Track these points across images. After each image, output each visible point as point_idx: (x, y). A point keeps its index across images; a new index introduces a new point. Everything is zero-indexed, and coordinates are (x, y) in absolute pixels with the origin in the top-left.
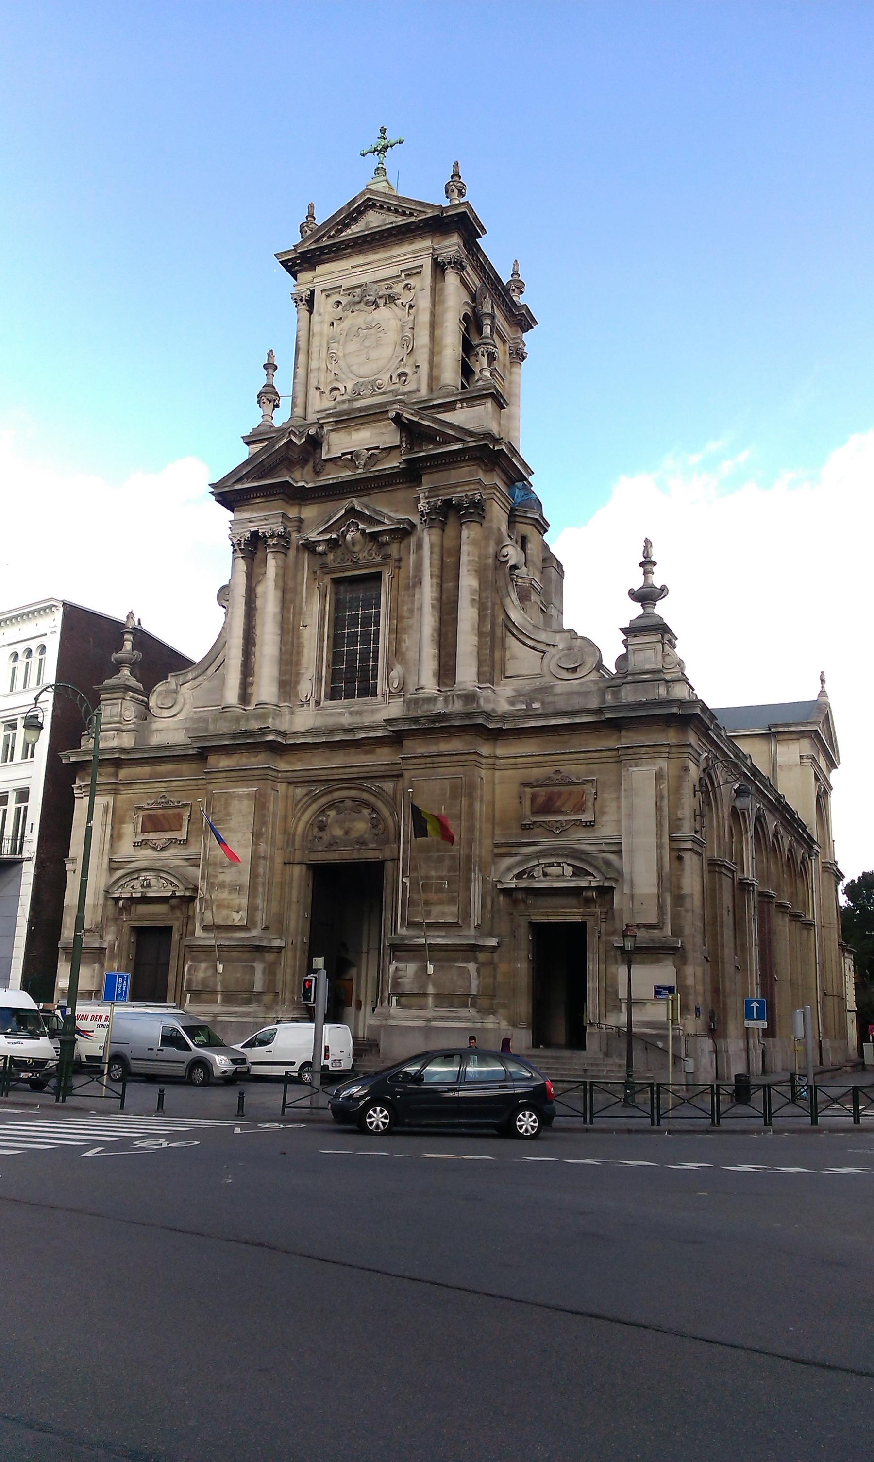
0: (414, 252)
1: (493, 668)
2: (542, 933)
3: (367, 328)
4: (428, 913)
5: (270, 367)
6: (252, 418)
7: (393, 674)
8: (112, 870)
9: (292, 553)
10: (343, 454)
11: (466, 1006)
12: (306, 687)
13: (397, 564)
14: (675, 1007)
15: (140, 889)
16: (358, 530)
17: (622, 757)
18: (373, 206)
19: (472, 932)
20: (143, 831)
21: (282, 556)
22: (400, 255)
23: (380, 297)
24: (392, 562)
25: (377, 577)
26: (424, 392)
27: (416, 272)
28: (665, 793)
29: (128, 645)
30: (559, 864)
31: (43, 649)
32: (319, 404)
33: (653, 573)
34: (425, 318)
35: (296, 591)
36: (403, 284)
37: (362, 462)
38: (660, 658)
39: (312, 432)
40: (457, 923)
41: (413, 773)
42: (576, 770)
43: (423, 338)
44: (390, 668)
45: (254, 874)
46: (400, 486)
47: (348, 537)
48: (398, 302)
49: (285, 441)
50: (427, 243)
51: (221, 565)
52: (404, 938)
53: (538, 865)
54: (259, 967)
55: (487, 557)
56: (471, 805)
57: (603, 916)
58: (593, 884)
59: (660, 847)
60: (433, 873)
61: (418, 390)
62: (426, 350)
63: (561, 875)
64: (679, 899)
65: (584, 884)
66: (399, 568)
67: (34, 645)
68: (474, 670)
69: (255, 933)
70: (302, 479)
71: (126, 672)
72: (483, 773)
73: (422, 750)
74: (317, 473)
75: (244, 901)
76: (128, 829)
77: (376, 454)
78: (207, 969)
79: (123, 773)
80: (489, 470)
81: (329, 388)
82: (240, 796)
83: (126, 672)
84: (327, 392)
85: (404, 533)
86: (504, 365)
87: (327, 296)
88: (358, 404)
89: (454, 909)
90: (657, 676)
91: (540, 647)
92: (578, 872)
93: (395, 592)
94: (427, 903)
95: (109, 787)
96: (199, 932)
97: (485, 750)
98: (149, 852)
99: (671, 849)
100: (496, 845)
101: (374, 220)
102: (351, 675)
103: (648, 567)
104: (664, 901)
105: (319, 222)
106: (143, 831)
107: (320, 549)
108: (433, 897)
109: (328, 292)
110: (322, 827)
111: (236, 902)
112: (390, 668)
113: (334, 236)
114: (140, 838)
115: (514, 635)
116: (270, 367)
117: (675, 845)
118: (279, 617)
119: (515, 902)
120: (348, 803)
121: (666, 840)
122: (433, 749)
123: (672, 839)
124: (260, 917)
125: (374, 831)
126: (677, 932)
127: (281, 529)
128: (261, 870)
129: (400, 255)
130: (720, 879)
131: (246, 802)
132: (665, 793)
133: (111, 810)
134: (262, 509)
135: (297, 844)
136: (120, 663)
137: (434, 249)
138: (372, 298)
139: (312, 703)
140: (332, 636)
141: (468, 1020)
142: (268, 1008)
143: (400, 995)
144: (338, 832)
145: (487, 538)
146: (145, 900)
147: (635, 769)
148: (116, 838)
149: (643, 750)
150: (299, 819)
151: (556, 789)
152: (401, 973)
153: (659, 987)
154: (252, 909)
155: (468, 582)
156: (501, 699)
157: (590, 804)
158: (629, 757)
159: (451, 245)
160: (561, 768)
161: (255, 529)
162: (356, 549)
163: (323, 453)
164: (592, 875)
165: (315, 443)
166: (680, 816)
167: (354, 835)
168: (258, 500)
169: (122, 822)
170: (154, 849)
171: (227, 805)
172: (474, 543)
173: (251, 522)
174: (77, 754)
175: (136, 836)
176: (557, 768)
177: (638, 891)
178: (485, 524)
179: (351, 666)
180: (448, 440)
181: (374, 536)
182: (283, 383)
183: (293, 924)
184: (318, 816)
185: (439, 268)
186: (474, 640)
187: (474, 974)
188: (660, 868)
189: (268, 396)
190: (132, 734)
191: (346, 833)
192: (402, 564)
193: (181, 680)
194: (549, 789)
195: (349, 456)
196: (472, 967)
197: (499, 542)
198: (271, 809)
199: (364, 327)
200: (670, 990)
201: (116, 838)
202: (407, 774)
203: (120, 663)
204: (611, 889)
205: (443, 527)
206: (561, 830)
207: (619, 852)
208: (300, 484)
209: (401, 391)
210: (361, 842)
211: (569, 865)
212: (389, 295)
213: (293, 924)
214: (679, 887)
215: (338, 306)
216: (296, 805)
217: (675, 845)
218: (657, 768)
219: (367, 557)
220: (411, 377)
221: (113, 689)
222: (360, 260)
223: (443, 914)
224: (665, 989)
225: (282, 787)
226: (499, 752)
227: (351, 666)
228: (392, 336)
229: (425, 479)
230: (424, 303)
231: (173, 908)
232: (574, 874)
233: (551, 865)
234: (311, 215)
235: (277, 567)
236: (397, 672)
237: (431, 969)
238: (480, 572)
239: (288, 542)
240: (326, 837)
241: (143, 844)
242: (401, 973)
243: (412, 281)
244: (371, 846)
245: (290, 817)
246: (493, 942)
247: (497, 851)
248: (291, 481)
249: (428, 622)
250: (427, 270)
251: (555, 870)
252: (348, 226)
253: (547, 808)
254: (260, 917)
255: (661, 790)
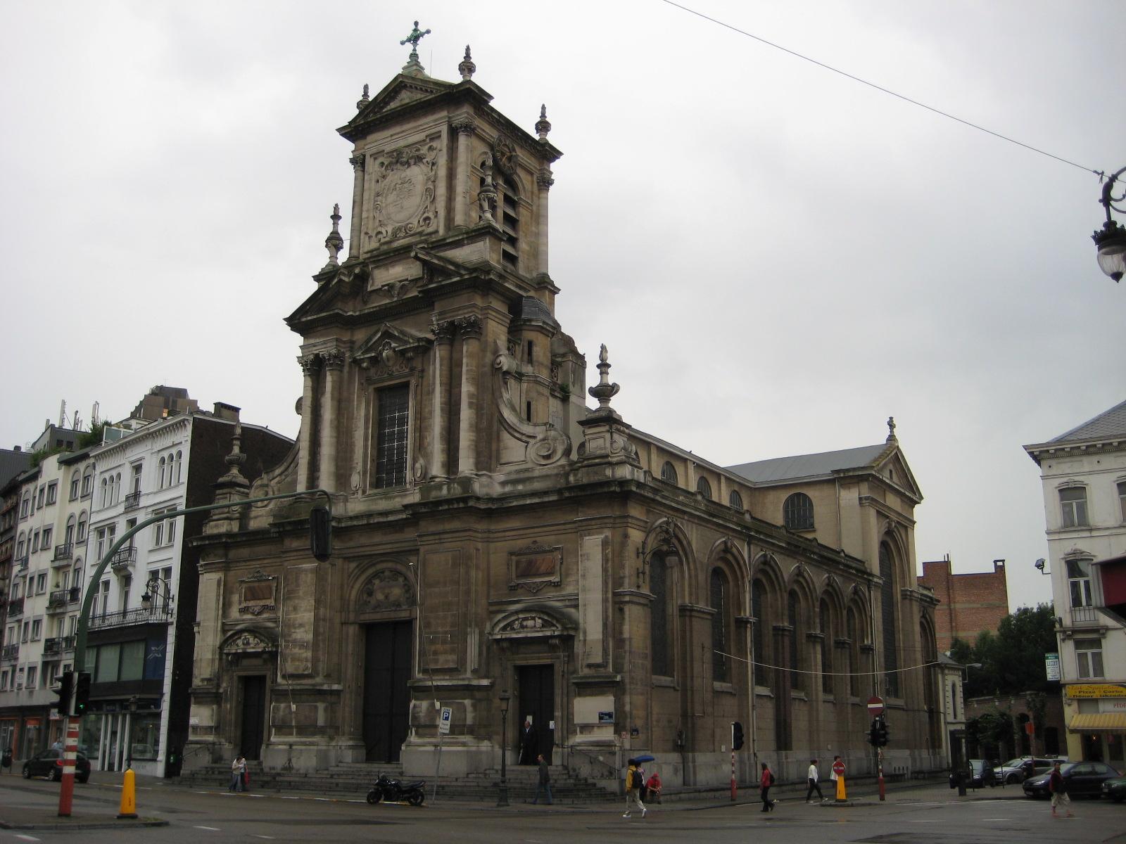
0: (435, 121)
1: (490, 458)
2: (522, 671)
3: (402, 183)
4: (436, 661)
5: (336, 217)
6: (321, 260)
7: (418, 465)
8: (224, 631)
9: (346, 369)
10: (383, 286)
11: (463, 734)
12: (355, 480)
13: (420, 375)
14: (113, 751)
15: (242, 646)
16: (391, 348)
17: (584, 529)
18: (405, 87)
19: (469, 675)
20: (245, 600)
21: (339, 373)
22: (425, 124)
23: (411, 158)
24: (416, 373)
25: (406, 386)
26: (441, 232)
27: (436, 137)
28: (610, 556)
29: (236, 450)
30: (533, 619)
31: (180, 454)
32: (370, 245)
33: (608, 374)
34: (442, 172)
35: (350, 401)
36: (427, 147)
37: (396, 292)
38: (608, 445)
39: (357, 271)
40: (456, 668)
41: (426, 547)
42: (548, 540)
43: (441, 190)
44: (415, 460)
45: (316, 633)
46: (423, 310)
47: (384, 354)
48: (424, 161)
49: (336, 280)
50: (444, 113)
51: (296, 383)
52: (420, 680)
53: (517, 620)
54: (321, 706)
55: (484, 366)
56: (467, 573)
57: (566, 659)
58: (556, 633)
59: (605, 600)
60: (440, 629)
61: (436, 232)
62: (444, 198)
63: (533, 628)
64: (620, 642)
65: (548, 633)
66: (422, 377)
67: (174, 451)
68: (472, 461)
69: (318, 680)
70: (351, 310)
71: (235, 471)
72: (480, 545)
73: (433, 529)
74: (365, 303)
75: (309, 654)
76: (235, 598)
77: (405, 285)
78: (285, 708)
79: (233, 554)
80: (485, 295)
81: (375, 232)
82: (306, 570)
83: (235, 471)
84: (374, 235)
85: (425, 348)
86: (532, 193)
87: (375, 159)
88: (396, 244)
89: (455, 657)
90: (606, 460)
91: (524, 438)
92: (546, 624)
93: (419, 397)
94: (435, 653)
95: (220, 565)
96: (279, 680)
97: (481, 526)
98: (249, 616)
99: (615, 603)
100: (491, 604)
101: (405, 97)
102: (387, 470)
103: (603, 369)
104: (608, 644)
105: (370, 99)
106: (245, 600)
107: (365, 365)
108: (439, 647)
109: (375, 156)
110: (370, 594)
111: (304, 655)
112: (415, 460)
113: (378, 112)
114: (244, 605)
115: (507, 430)
116: (336, 217)
117: (617, 599)
118: (336, 423)
119: (503, 650)
120: (387, 573)
121: (610, 595)
122: (440, 527)
123: (615, 594)
124: (322, 667)
125: (407, 595)
126: (618, 669)
127: (334, 351)
128: (321, 630)
129: (425, 124)
130: (691, 622)
131: (310, 575)
132: (610, 556)
133: (222, 583)
134: (322, 336)
135: (351, 608)
136: (231, 463)
137: (449, 118)
138: (405, 160)
139: (360, 492)
140: (376, 435)
141: (464, 744)
142: (331, 739)
143: (418, 727)
144: (380, 596)
145: (484, 350)
146: (246, 655)
147: (587, 538)
148: (226, 606)
149: (593, 522)
150: (352, 587)
151: (533, 557)
152: (418, 710)
153: (602, 714)
154: (315, 661)
155: (466, 388)
156: (491, 485)
157: (558, 568)
158: (583, 528)
159: (464, 114)
160: (538, 539)
161: (317, 352)
162: (391, 363)
163: (369, 287)
164: (554, 626)
165: (364, 278)
166: (622, 575)
167: (392, 599)
168: (319, 329)
169: (232, 593)
170: (253, 614)
171: (297, 579)
172: (470, 355)
173: (315, 346)
174: (197, 540)
175: (240, 604)
176: (534, 539)
177: (589, 637)
178: (483, 339)
179: (390, 460)
180: (448, 274)
181: (403, 352)
182: (345, 231)
183: (349, 672)
184: (367, 584)
185: (453, 133)
186: (472, 436)
187: (469, 709)
188: (605, 618)
189: (334, 242)
190: (237, 521)
191: (386, 597)
192: (425, 374)
193: (271, 475)
194: (529, 557)
195: (386, 288)
196: (467, 702)
197: (496, 354)
198: (329, 580)
199: (399, 182)
200: (610, 715)
201: (226, 606)
202: (422, 550)
203: (231, 463)
204: (571, 638)
205: (451, 343)
206: (537, 590)
207: (576, 606)
208: (349, 314)
209: (426, 232)
210: (397, 605)
211: (539, 618)
212: (418, 156)
213: (349, 672)
214: (621, 633)
215: (382, 166)
216: (349, 576)
217: (617, 599)
218: (603, 536)
219: (398, 371)
220: (433, 221)
221: (223, 485)
222: (397, 129)
223: (447, 661)
224: (606, 714)
225: (339, 562)
226: (493, 527)
227: (390, 460)
228: (419, 188)
229: (437, 305)
230: (442, 161)
231: (265, 661)
232: (543, 626)
233: (526, 619)
234: (366, 95)
235: (333, 382)
236: (421, 461)
237: (294, 707)
238: (478, 381)
239: (342, 361)
240: (373, 602)
241: (244, 611)
242: (418, 710)
243: (434, 144)
244: (404, 607)
245: (346, 586)
246: (485, 682)
247: (492, 608)
248: (341, 312)
249: (437, 423)
250: (445, 135)
251: (530, 623)
252: (387, 103)
253: (525, 574)
254: (322, 667)
255: (606, 555)
